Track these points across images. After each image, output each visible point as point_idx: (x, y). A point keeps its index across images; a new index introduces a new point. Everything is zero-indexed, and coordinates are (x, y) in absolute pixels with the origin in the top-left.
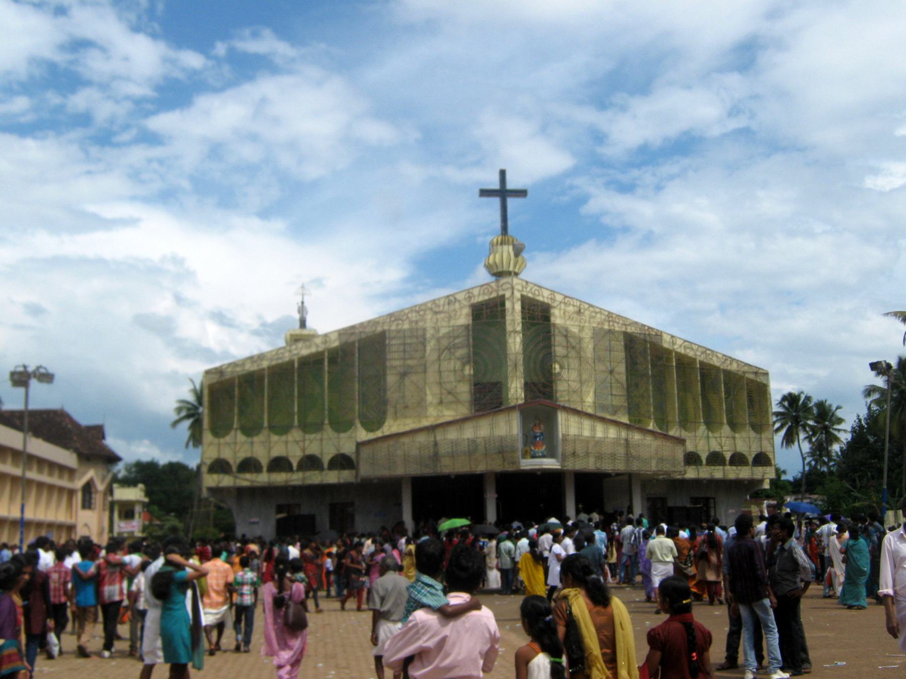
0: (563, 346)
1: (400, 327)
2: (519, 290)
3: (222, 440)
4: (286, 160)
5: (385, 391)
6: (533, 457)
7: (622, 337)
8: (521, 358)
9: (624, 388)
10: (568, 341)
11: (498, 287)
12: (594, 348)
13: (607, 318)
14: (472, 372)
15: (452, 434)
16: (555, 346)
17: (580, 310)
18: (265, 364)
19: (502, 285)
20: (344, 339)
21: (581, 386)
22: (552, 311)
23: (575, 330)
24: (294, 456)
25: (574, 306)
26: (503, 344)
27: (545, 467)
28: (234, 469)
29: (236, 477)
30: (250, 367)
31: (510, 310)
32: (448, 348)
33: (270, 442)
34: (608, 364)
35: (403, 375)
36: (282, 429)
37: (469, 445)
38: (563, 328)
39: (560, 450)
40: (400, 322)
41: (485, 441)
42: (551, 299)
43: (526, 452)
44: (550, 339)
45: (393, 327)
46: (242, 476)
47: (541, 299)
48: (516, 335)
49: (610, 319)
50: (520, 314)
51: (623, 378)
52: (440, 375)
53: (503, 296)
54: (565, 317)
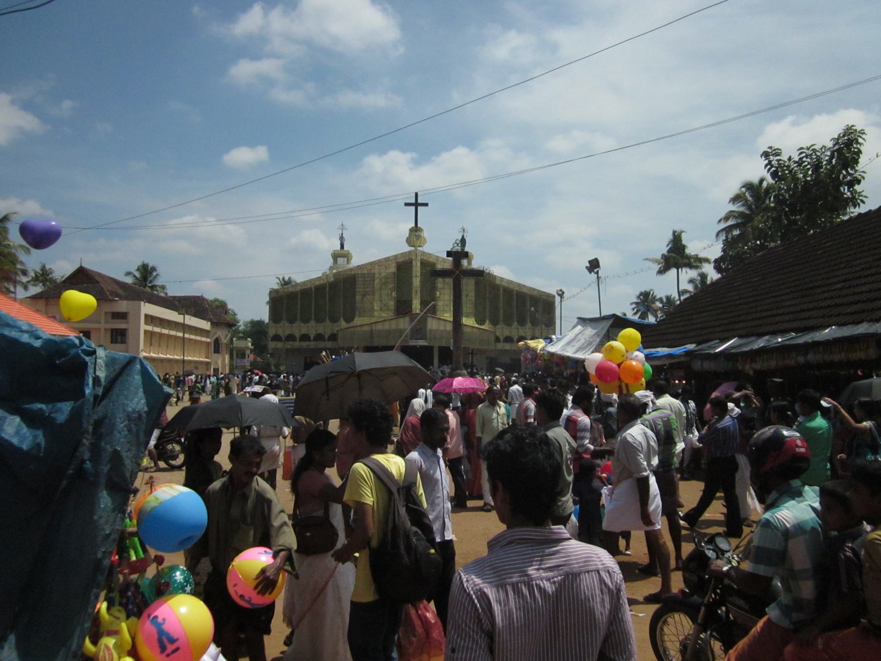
3: (278, 325)
5: (355, 303)
26: (411, 283)
32: (385, 284)
35: (364, 295)
39: (428, 336)
51: (473, 299)
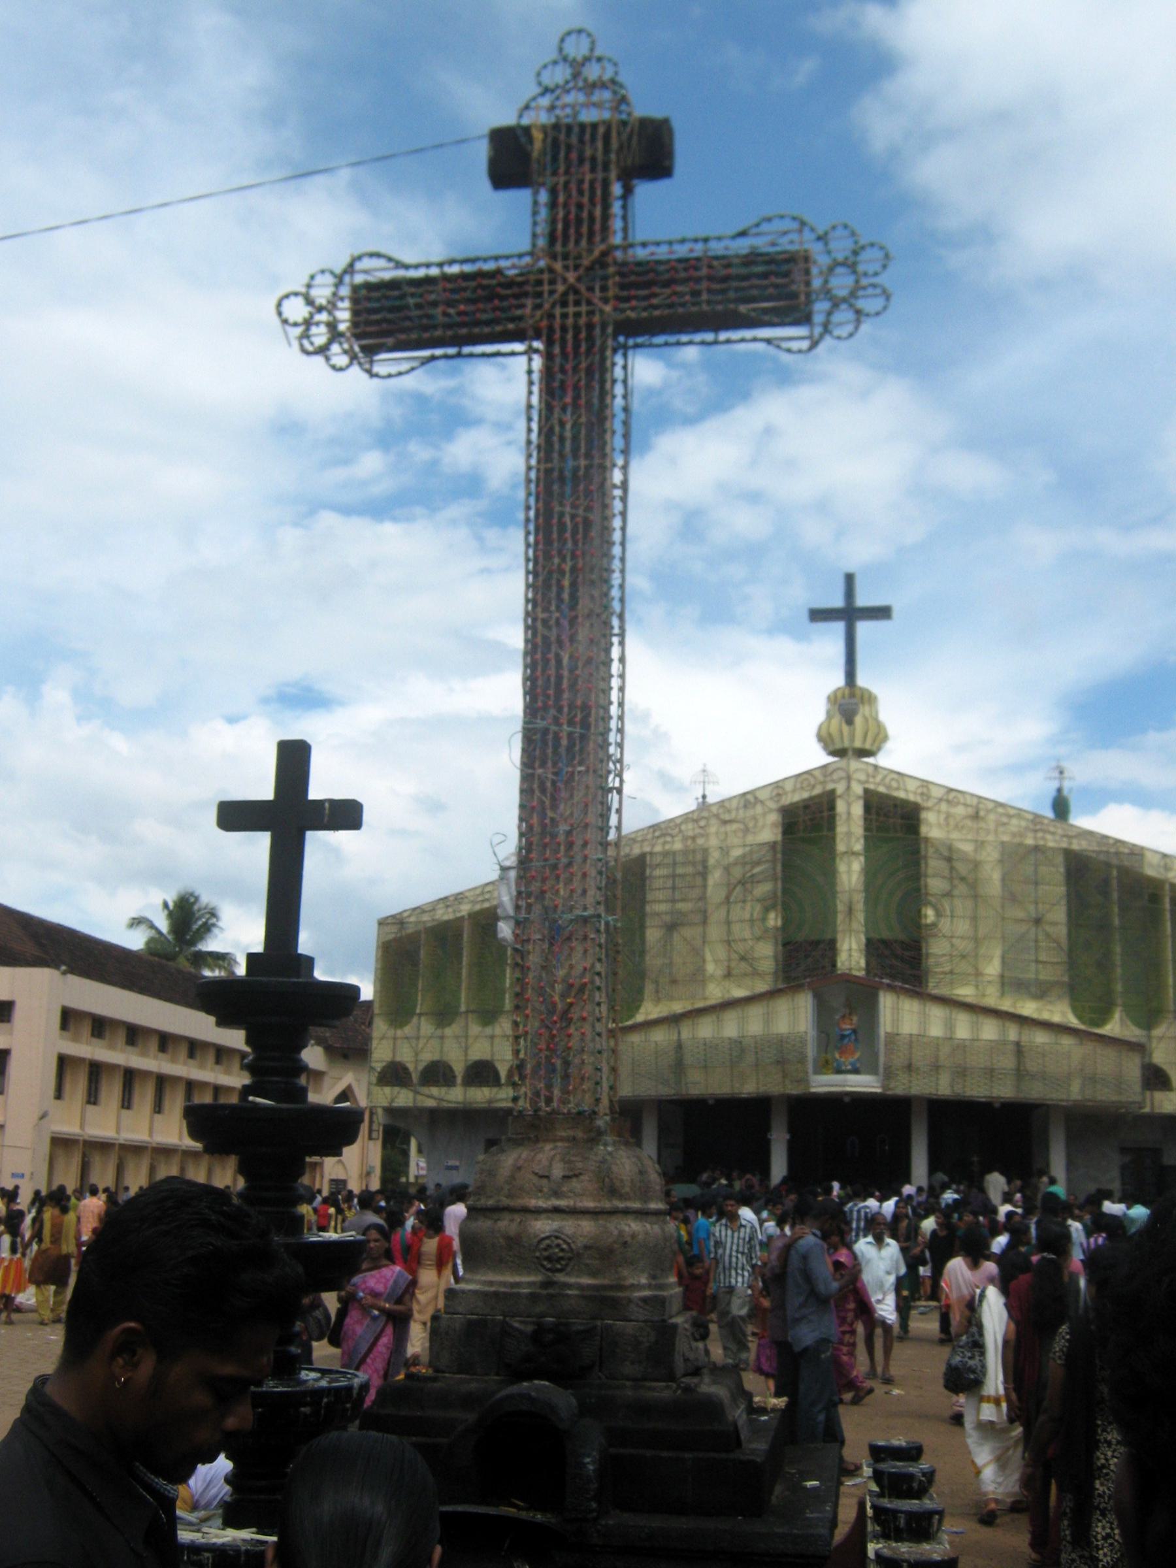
0: (943, 877)
1: (667, 847)
2: (859, 781)
3: (399, 1033)
4: (814, 533)
5: (643, 953)
6: (839, 1071)
7: (1060, 859)
8: (859, 900)
9: (1062, 949)
10: (952, 868)
11: (825, 776)
12: (1003, 880)
13: (1031, 826)
14: (779, 923)
15: (730, 1027)
16: (926, 876)
17: (977, 813)
18: (465, 909)
19: (832, 773)
21: (976, 947)
22: (924, 815)
23: (967, 848)
24: (504, 1060)
25: (966, 805)
26: (830, 873)
27: (849, 1089)
28: (415, 1077)
29: (416, 1092)
30: (444, 915)
31: (844, 817)
32: (742, 882)
33: (467, 1037)
34: (1032, 908)
35: (671, 927)
36: (444, 1015)
37: (731, 1049)
40: (668, 839)
41: (756, 1043)
42: (922, 794)
43: (827, 1062)
45: (658, 849)
46: (425, 1090)
47: (901, 795)
48: (853, 858)
49: (1038, 827)
50: (861, 822)
51: (1061, 931)
52: (729, 926)
53: (833, 792)
54: (948, 824)
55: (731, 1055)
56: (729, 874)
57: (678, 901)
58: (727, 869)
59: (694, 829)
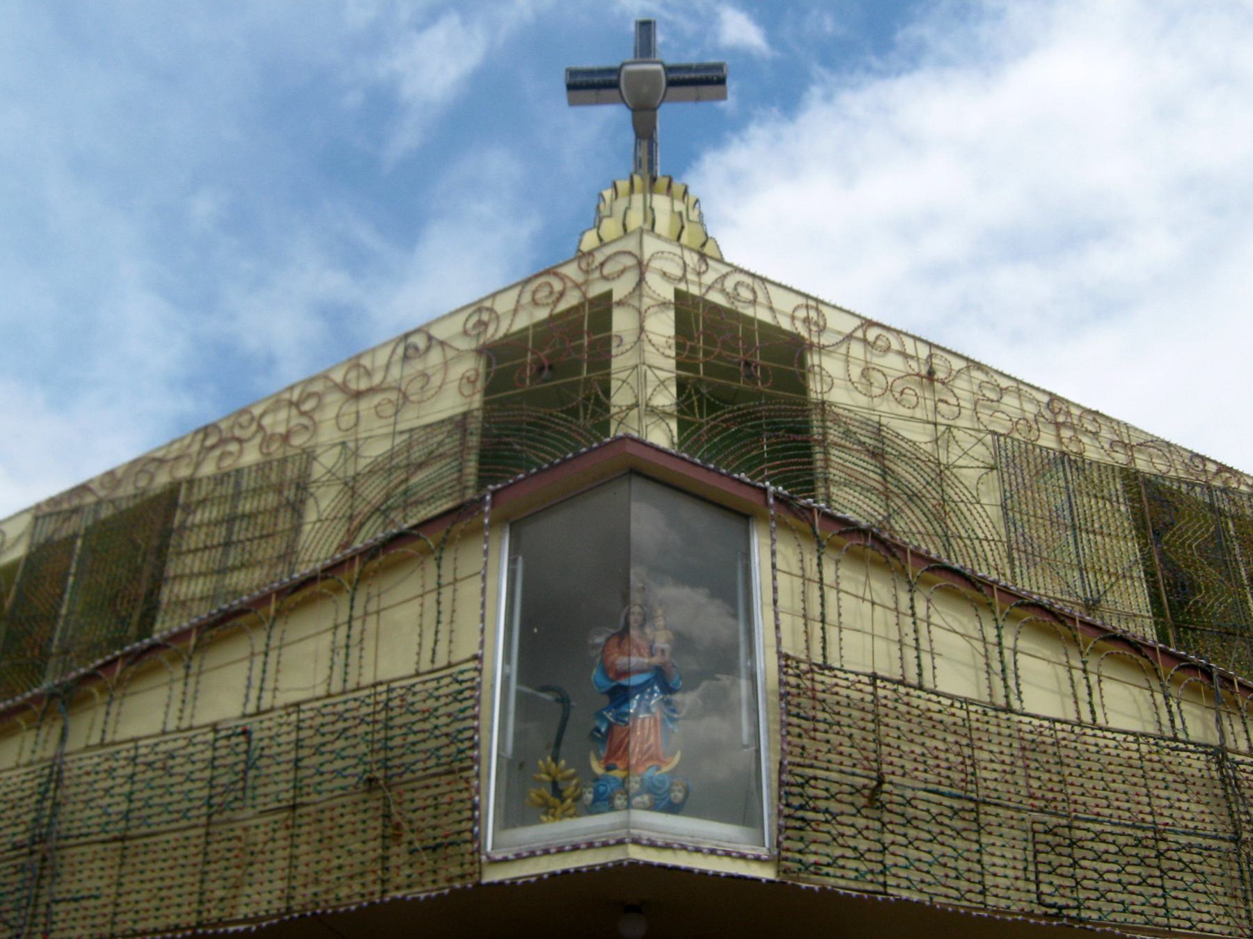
1: (227, 463)
10: (885, 472)
19: (602, 265)
20: (48, 528)
22: (813, 359)
23: (919, 435)
25: (904, 354)
31: (629, 339)
38: (865, 423)
40: (233, 447)
44: (810, 455)
47: (763, 315)
55: (211, 783)
56: (354, 493)
57: (233, 569)
58: (351, 486)
59: (288, 420)
